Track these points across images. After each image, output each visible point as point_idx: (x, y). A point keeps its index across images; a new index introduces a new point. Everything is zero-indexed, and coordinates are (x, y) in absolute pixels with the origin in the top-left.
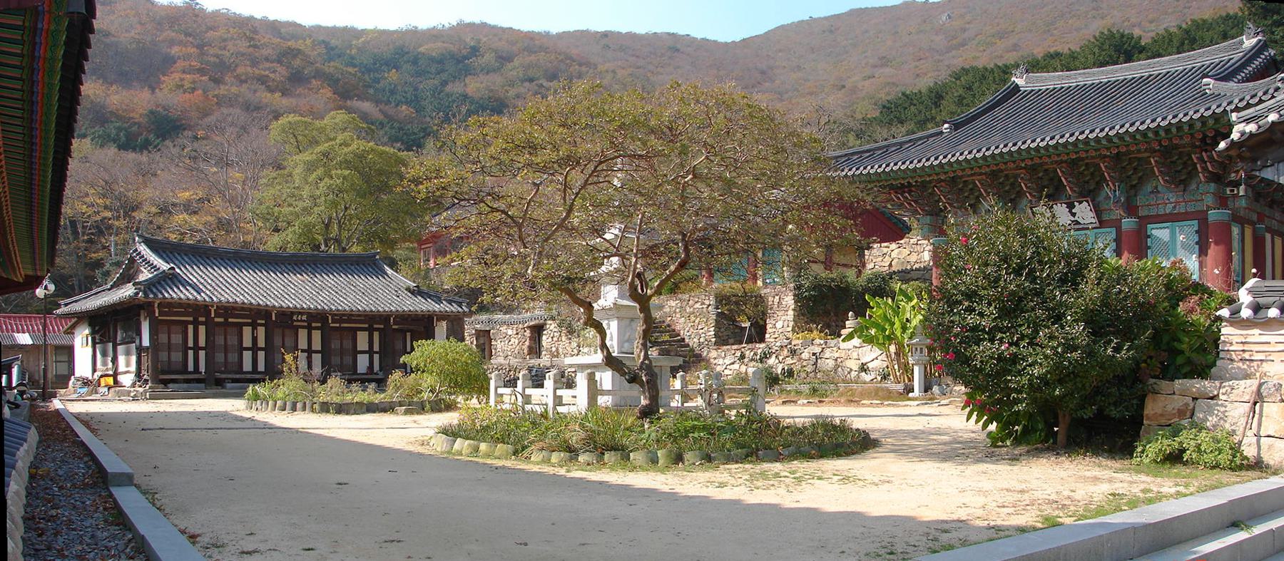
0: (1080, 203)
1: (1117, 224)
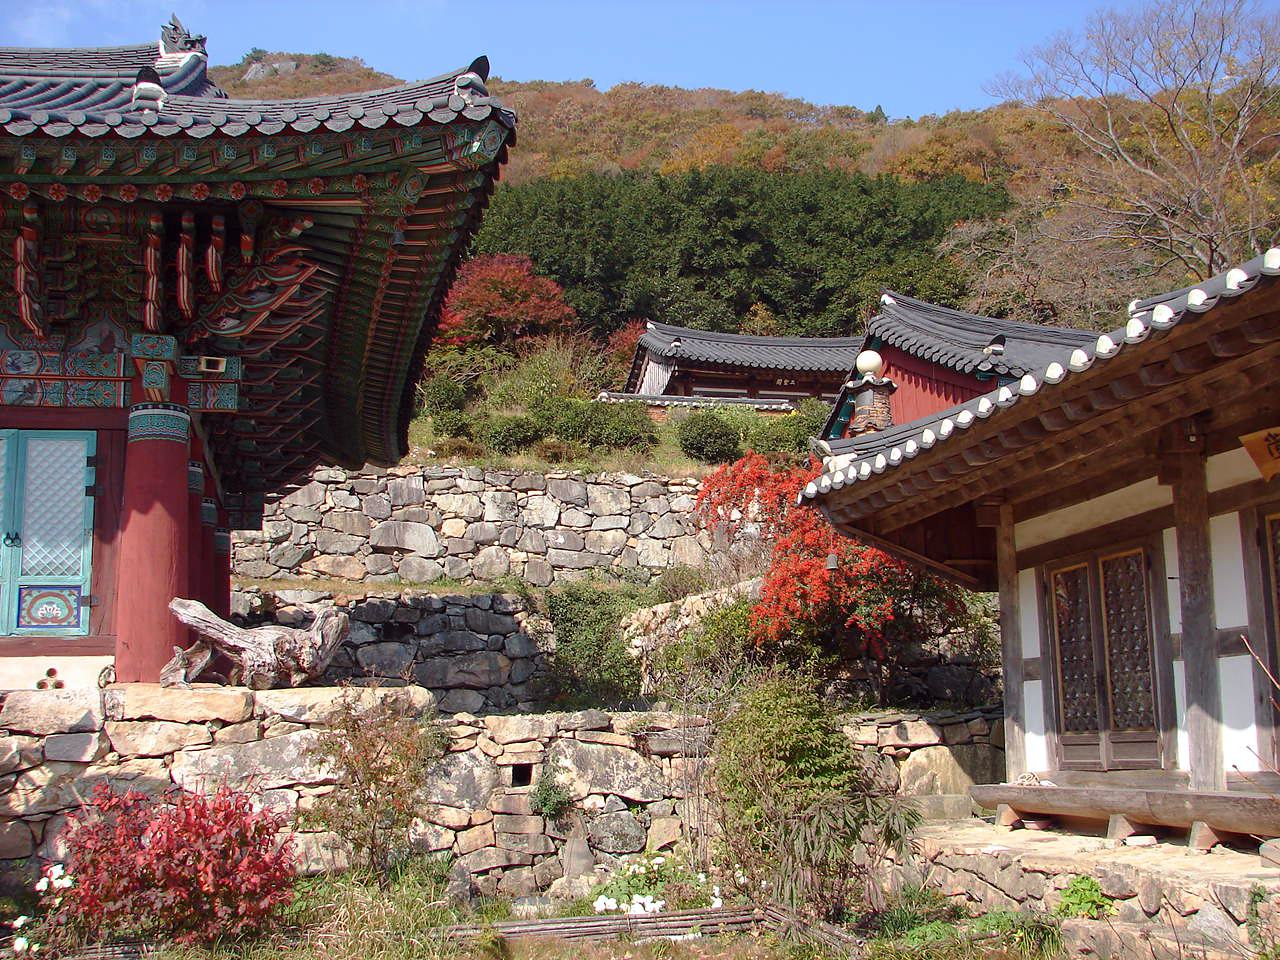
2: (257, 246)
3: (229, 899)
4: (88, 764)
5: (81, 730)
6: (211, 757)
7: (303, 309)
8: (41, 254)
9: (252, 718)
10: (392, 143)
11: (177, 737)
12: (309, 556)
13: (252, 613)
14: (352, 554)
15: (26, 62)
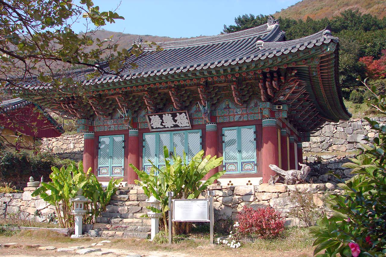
0: (180, 114)
1: (203, 128)
2: (285, 78)
3: (269, 230)
4: (252, 202)
5: (249, 194)
6: (278, 201)
7: (299, 91)
8: (238, 87)
9: (287, 191)
10: (309, 52)
11: (270, 196)
12: (330, 145)
13: (315, 162)
14: (342, 144)
15: (238, 35)
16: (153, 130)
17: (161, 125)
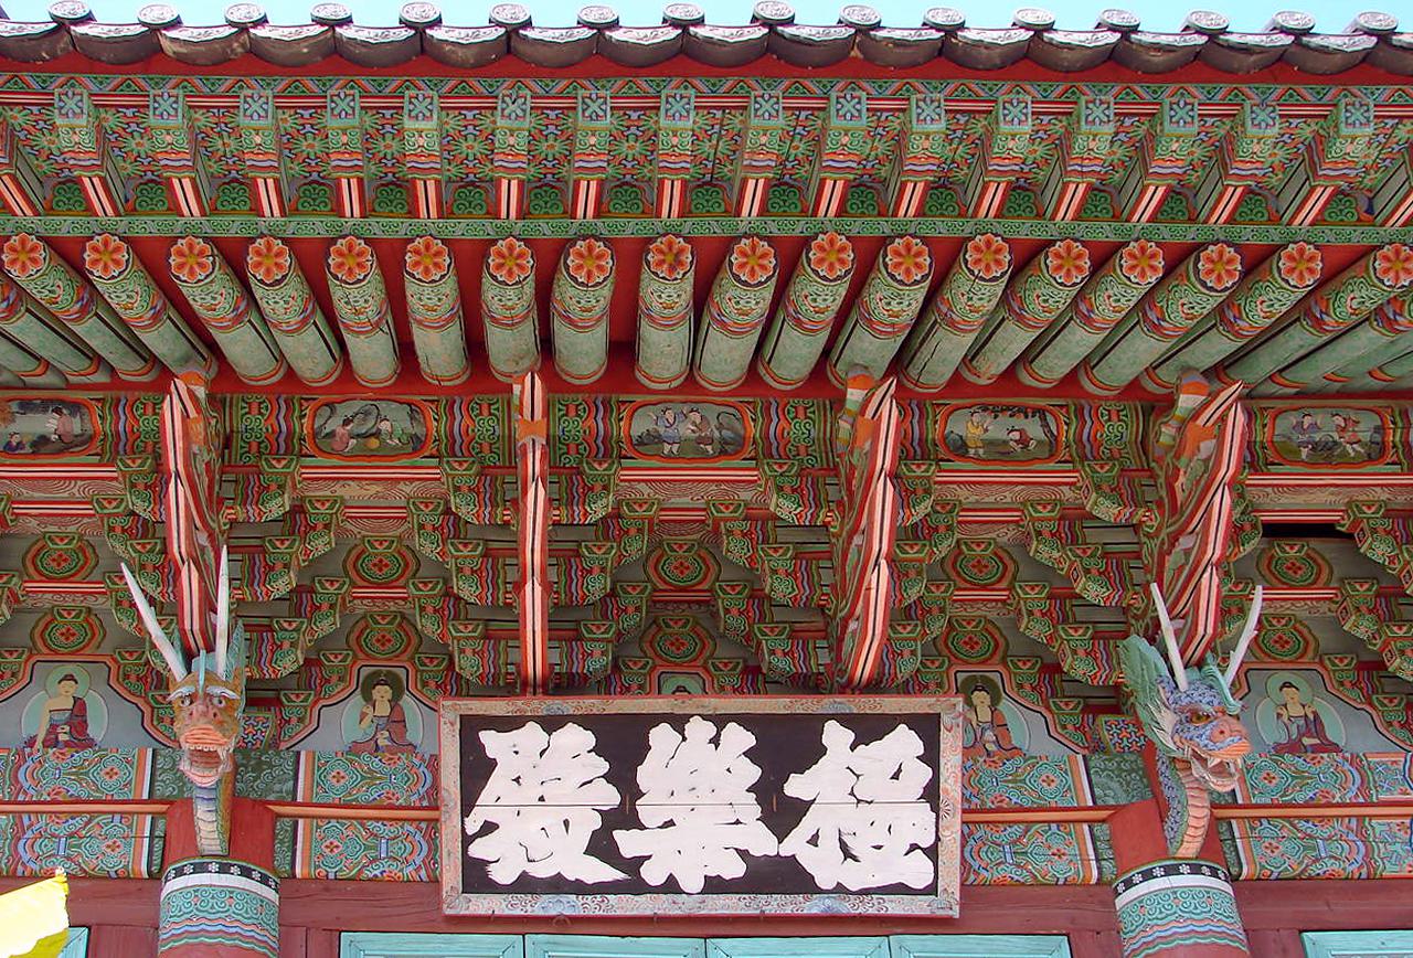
0: (868, 730)
16: (482, 904)
17: (601, 846)
